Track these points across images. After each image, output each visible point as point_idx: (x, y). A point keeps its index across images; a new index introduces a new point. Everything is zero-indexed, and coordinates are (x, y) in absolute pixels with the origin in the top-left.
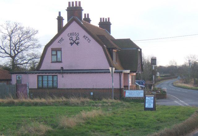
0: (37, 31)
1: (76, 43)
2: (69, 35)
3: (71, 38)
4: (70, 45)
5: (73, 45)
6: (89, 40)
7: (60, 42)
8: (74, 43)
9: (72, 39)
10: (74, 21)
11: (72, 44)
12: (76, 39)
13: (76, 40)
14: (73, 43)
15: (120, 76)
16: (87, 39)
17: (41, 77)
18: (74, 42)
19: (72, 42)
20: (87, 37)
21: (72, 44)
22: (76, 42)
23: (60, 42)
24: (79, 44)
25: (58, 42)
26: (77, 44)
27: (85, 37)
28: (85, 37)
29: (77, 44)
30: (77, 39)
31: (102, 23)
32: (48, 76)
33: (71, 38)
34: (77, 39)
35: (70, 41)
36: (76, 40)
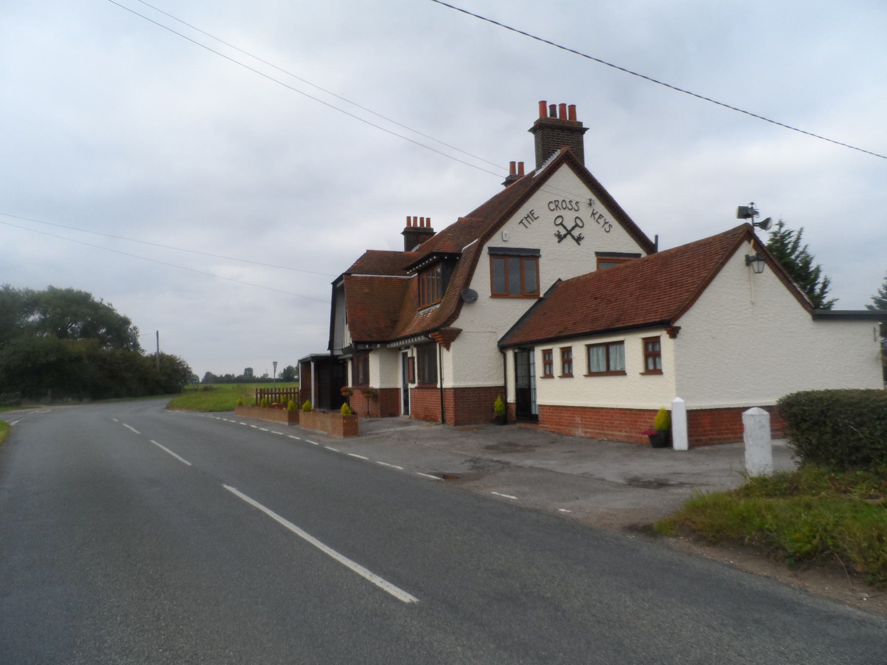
0: (802, 229)
1: (573, 237)
2: (553, 206)
3: (559, 221)
4: (556, 239)
5: (564, 240)
6: (607, 226)
7: (525, 221)
8: (569, 237)
9: (561, 224)
10: (370, 355)
11: (561, 238)
12: (574, 224)
13: (573, 228)
14: (565, 236)
15: (524, 224)
16: (602, 221)
17: (601, 351)
18: (569, 232)
19: (563, 232)
20: (601, 216)
21: (561, 238)
22: (576, 233)
23: (525, 221)
24: (582, 242)
25: (521, 222)
26: (578, 240)
27: (597, 216)
28: (597, 216)
29: (578, 240)
30: (577, 225)
31: (415, 228)
32: (607, 345)
33: (581, 225)
34: (577, 225)
35: (555, 229)
36: (573, 228)
